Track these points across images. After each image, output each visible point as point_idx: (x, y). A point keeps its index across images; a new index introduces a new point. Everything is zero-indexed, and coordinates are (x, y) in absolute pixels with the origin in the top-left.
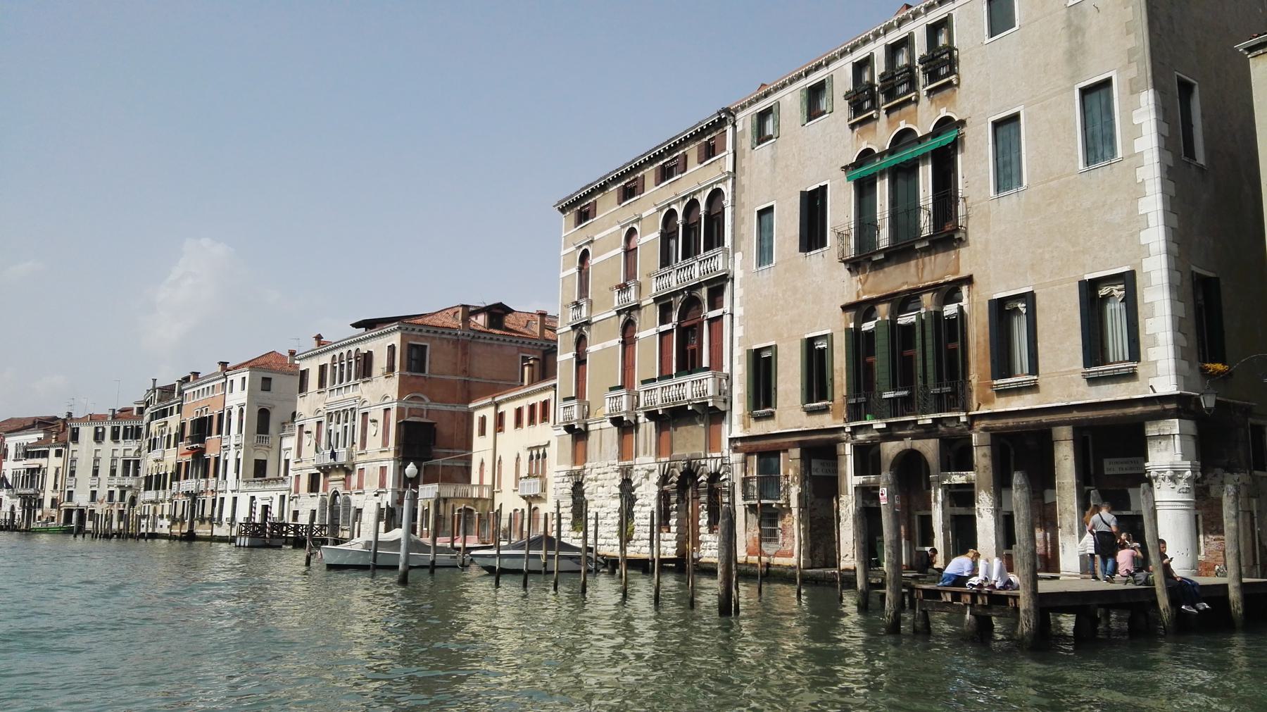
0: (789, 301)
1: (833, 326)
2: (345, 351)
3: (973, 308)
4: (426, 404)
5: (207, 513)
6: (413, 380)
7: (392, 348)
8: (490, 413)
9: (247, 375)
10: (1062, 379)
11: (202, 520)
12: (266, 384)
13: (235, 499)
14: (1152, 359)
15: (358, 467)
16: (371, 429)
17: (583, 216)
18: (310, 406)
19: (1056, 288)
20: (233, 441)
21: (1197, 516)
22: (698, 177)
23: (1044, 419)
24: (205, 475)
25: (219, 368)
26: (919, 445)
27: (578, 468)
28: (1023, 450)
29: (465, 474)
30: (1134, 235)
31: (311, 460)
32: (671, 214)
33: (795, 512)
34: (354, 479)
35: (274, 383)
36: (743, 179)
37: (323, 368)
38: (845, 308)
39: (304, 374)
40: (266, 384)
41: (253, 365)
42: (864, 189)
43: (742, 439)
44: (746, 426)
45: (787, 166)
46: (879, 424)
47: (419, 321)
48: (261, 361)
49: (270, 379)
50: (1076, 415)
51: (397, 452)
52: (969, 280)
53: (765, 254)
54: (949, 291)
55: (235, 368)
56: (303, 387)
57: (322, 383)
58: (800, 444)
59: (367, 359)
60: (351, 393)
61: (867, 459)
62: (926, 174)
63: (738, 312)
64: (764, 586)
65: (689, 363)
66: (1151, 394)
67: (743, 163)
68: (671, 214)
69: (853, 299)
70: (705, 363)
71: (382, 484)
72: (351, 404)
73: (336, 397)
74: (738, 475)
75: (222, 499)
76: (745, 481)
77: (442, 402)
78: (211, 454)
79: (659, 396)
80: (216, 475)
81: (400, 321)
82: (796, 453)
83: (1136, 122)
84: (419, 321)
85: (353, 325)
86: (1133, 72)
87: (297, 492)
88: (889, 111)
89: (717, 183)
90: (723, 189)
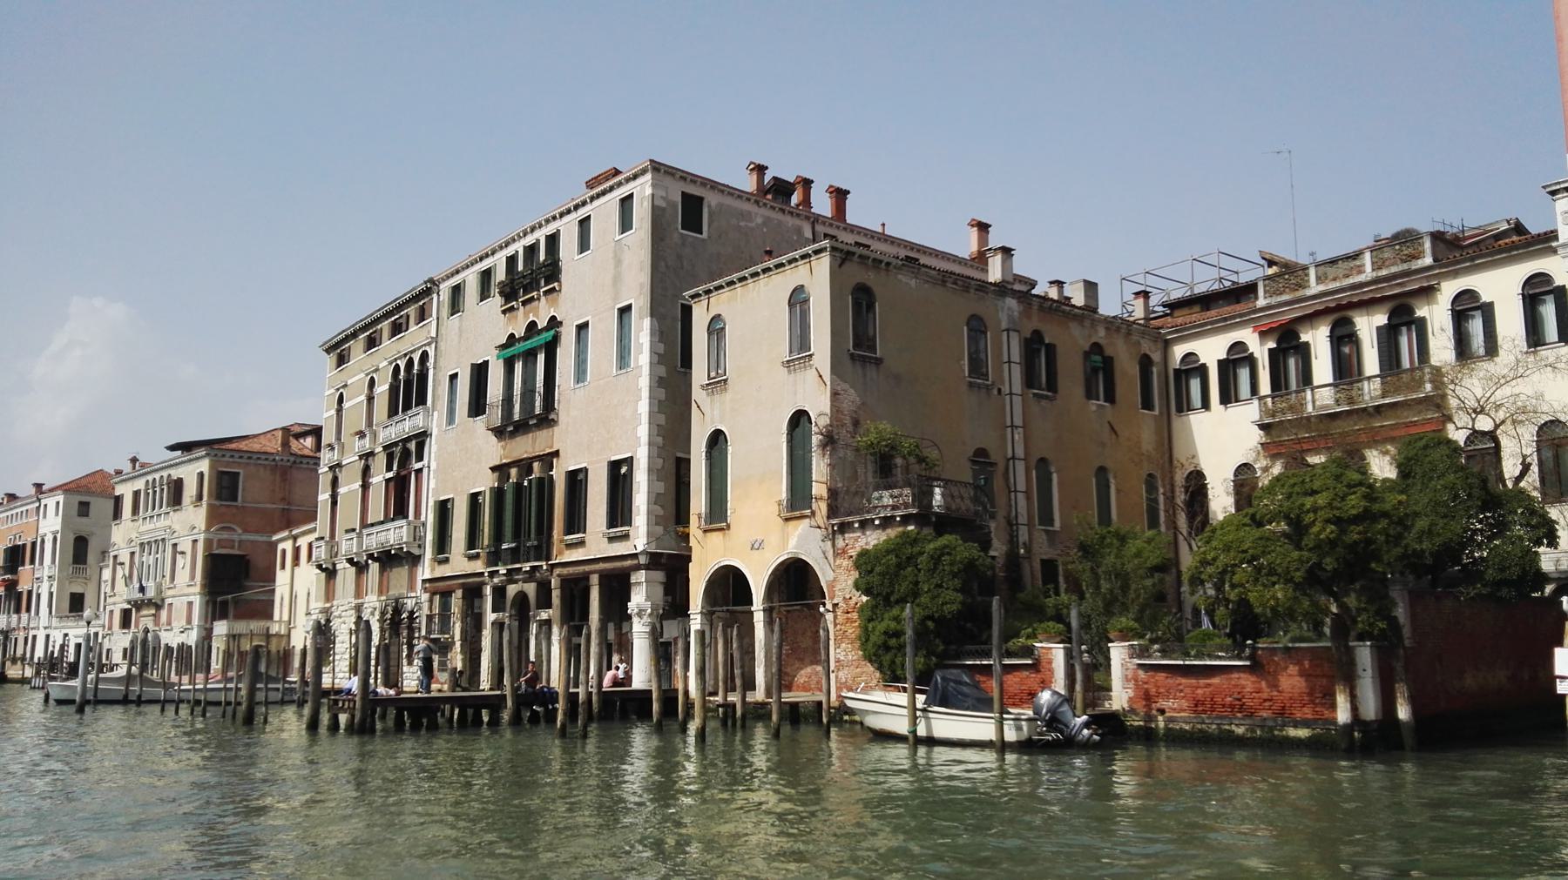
0: (463, 460)
1: (485, 483)
2: (157, 476)
3: (559, 474)
4: (238, 535)
5: (19, 652)
6: (223, 510)
7: (201, 475)
8: (288, 546)
9: (61, 498)
11: (14, 661)
12: (84, 509)
13: (48, 637)
15: (168, 601)
16: (180, 560)
17: (553, 318)
18: (124, 535)
20: (46, 573)
22: (415, 337)
23: (581, 569)
24: (18, 611)
25: (33, 491)
29: (264, 610)
31: (122, 595)
32: (397, 368)
33: (458, 644)
34: (164, 614)
35: (92, 507)
36: (442, 345)
37: (136, 494)
38: (493, 469)
39: (118, 500)
40: (84, 509)
41: (67, 488)
42: (509, 365)
44: (433, 570)
47: (233, 446)
48: (84, 482)
49: (87, 504)
50: (602, 566)
51: (204, 586)
53: (451, 419)
55: (51, 490)
56: (117, 514)
57: (135, 510)
59: (177, 487)
60: (163, 522)
62: (541, 358)
63: (433, 466)
64: (905, 712)
65: (401, 512)
67: (443, 331)
68: (397, 368)
69: (497, 463)
71: (189, 621)
72: (159, 535)
73: (149, 526)
74: (426, 611)
75: (34, 637)
76: (430, 618)
77: (257, 532)
78: (23, 587)
79: (375, 540)
80: (28, 610)
81: (210, 445)
82: (459, 593)
84: (233, 446)
85: (172, 448)
87: (110, 628)
88: (524, 303)
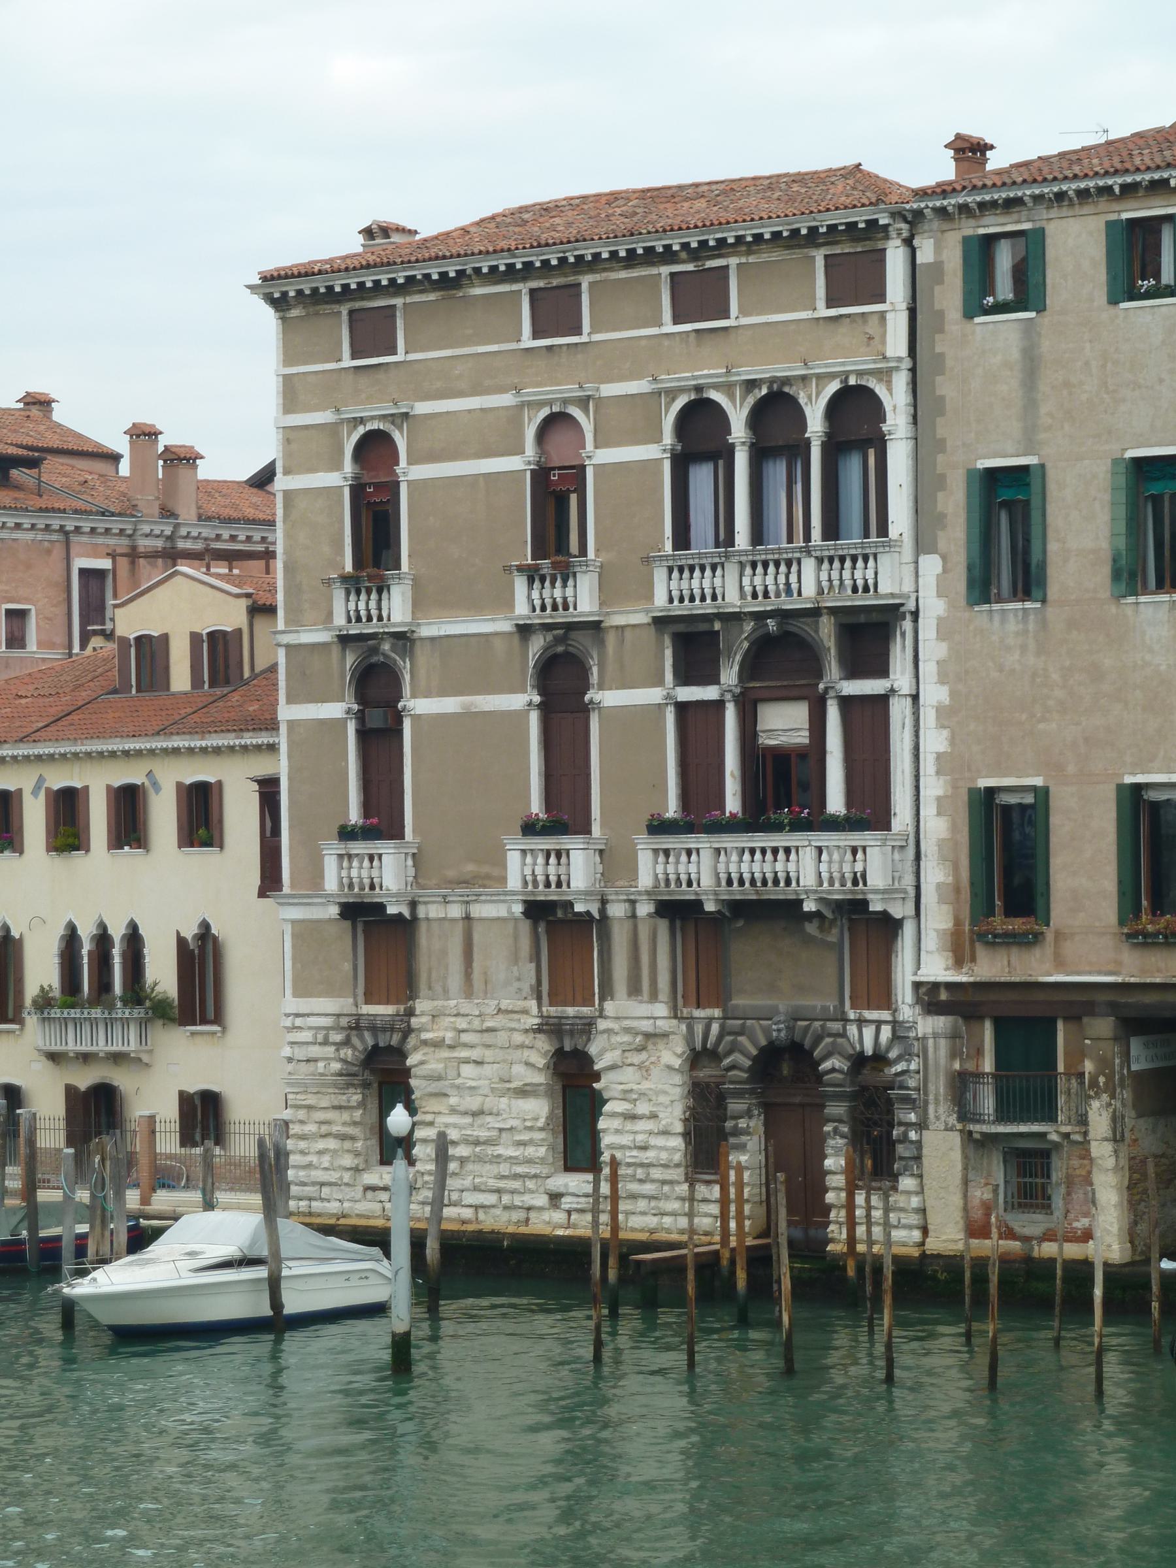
27: (148, 1003)
44: (960, 956)
45: (1067, 384)
58: (1114, 1008)
63: (934, 694)
70: (836, 803)
90: (880, 390)
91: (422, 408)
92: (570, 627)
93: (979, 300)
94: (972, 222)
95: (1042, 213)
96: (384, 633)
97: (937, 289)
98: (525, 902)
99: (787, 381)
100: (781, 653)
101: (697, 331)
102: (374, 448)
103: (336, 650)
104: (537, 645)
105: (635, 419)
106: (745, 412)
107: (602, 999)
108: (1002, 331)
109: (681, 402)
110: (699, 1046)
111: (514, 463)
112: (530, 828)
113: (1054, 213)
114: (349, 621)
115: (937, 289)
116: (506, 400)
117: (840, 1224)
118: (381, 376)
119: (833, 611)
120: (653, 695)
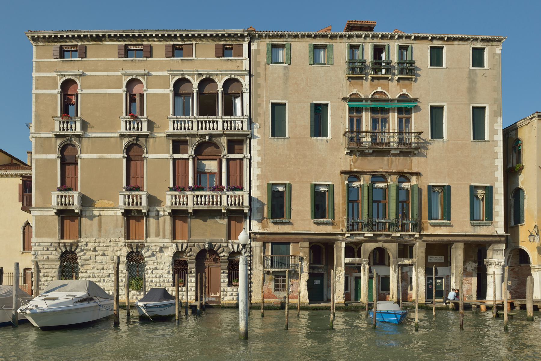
10: (461, 224)
14: (496, 220)
19: (459, 186)
21: (354, 264)
26: (386, 245)
28: (440, 250)
30: (492, 173)
38: (343, 173)
43: (260, 234)
45: (296, 83)
46: (369, 234)
52: (418, 174)
54: (404, 177)
61: (352, 250)
63: (256, 159)
66: (495, 234)
69: (348, 169)
70: (191, 184)
83: (495, 128)
86: (495, 108)
89: (238, 75)
90: (241, 80)
91: (88, 74)
92: (139, 136)
93: (273, 60)
94: (269, 40)
95: (290, 40)
96: (73, 135)
97: (258, 56)
98: (125, 209)
99: (212, 75)
100: (206, 146)
101: (182, 60)
102: (67, 84)
103: (54, 140)
104: (126, 141)
105: (162, 82)
106: (198, 82)
107: (147, 237)
108: (277, 69)
109: (177, 78)
110: (180, 250)
111: (120, 91)
112: (171, 189)
113: (294, 40)
114: (60, 130)
115: (258, 56)
116: (119, 73)
117: (302, 259)
118: (72, 63)
119: (227, 135)
120: (167, 156)
